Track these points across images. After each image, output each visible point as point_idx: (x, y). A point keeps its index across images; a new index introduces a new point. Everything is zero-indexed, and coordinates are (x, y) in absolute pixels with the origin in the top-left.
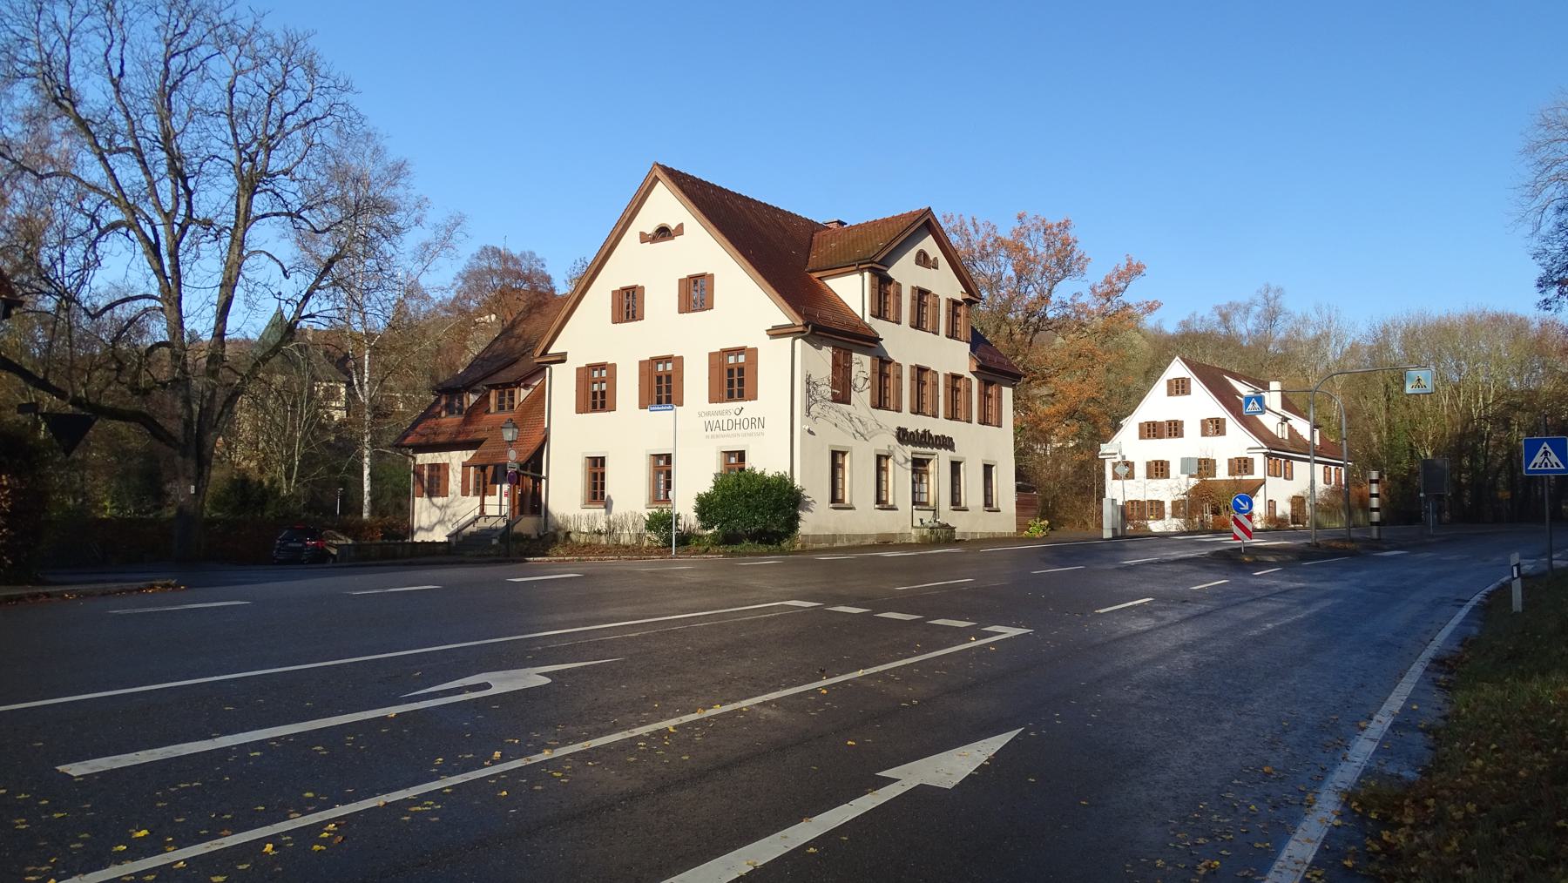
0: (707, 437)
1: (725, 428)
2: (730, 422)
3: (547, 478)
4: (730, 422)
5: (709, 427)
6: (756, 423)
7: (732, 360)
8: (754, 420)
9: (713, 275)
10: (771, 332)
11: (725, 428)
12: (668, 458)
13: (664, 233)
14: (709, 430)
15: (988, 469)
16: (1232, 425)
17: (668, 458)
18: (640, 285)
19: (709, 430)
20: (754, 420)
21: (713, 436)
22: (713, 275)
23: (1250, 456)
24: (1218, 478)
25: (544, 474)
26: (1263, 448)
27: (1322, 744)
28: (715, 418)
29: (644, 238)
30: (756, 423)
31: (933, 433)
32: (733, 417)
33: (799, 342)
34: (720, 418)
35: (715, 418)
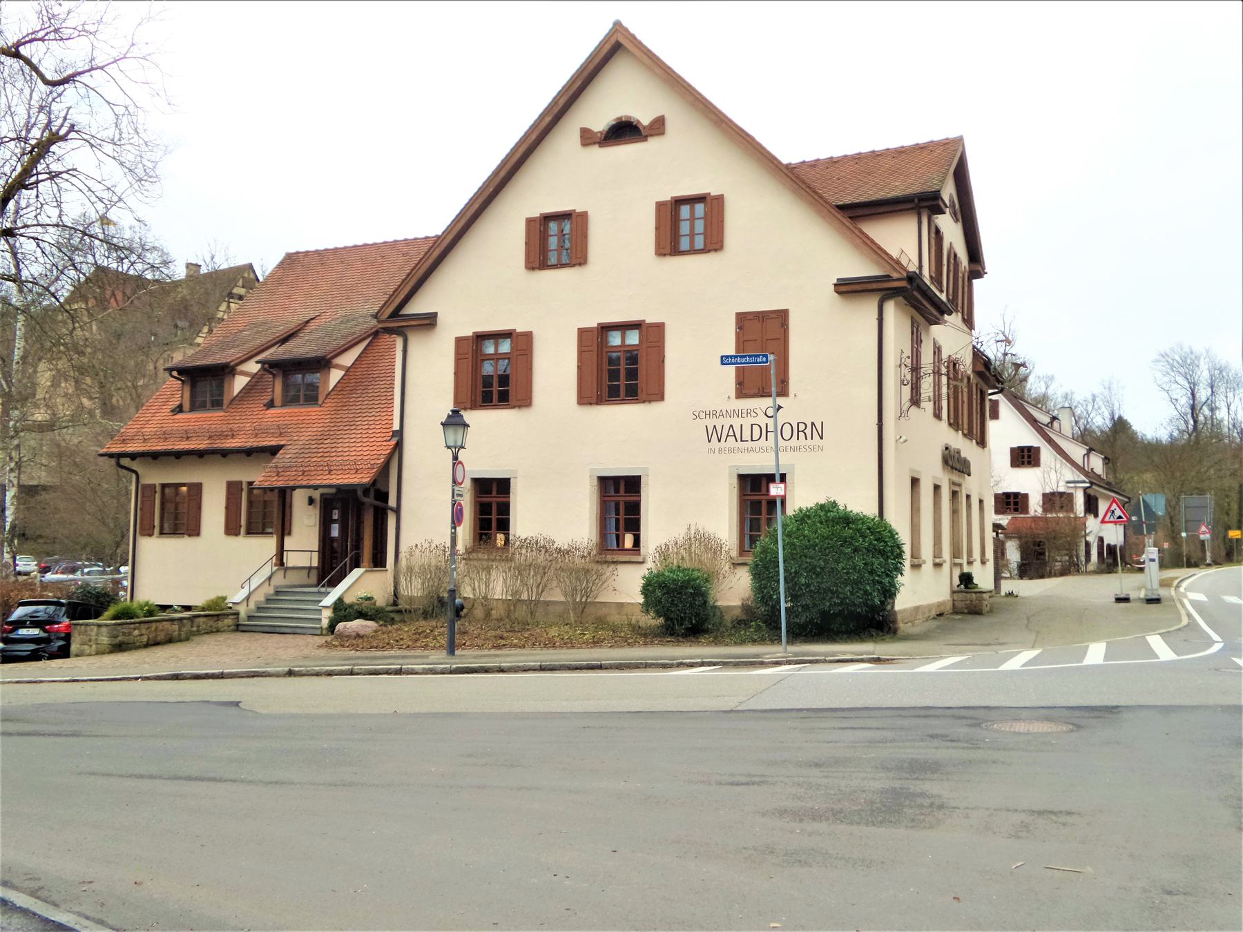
0: (711, 451)
1: (746, 435)
2: (756, 429)
3: (397, 511)
4: (756, 429)
5: (713, 435)
6: (808, 431)
7: (615, 339)
8: (802, 427)
9: (586, 213)
10: (843, 289)
11: (746, 435)
12: (632, 484)
13: (624, 131)
14: (715, 438)
15: (981, 502)
16: (1047, 454)
17: (632, 484)
18: (714, 193)
19: (715, 438)
20: (802, 427)
21: (720, 451)
22: (586, 213)
23: (1069, 491)
24: (1032, 513)
25: (392, 502)
26: (1084, 482)
27: (774, 784)
28: (727, 422)
29: (588, 138)
30: (808, 431)
31: (963, 455)
32: (762, 420)
33: (890, 308)
34: (736, 422)
35: (727, 422)
